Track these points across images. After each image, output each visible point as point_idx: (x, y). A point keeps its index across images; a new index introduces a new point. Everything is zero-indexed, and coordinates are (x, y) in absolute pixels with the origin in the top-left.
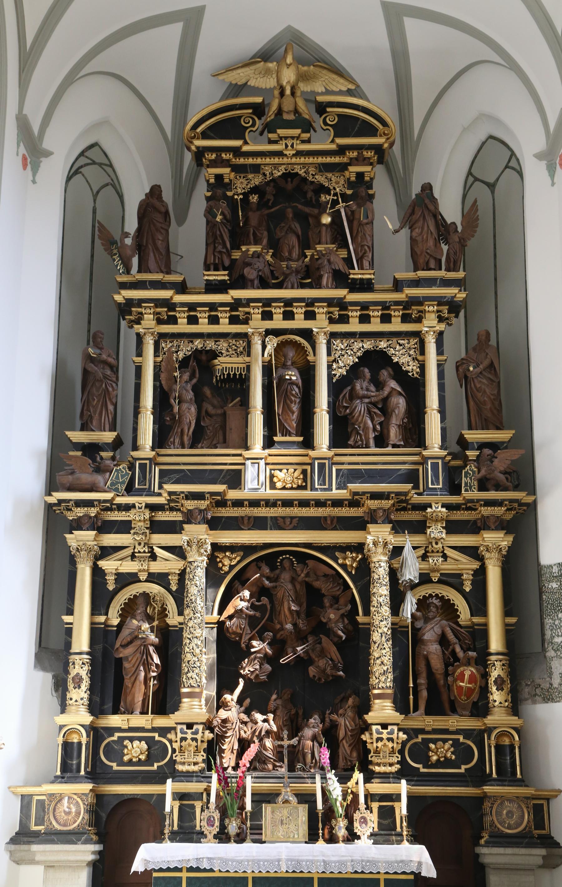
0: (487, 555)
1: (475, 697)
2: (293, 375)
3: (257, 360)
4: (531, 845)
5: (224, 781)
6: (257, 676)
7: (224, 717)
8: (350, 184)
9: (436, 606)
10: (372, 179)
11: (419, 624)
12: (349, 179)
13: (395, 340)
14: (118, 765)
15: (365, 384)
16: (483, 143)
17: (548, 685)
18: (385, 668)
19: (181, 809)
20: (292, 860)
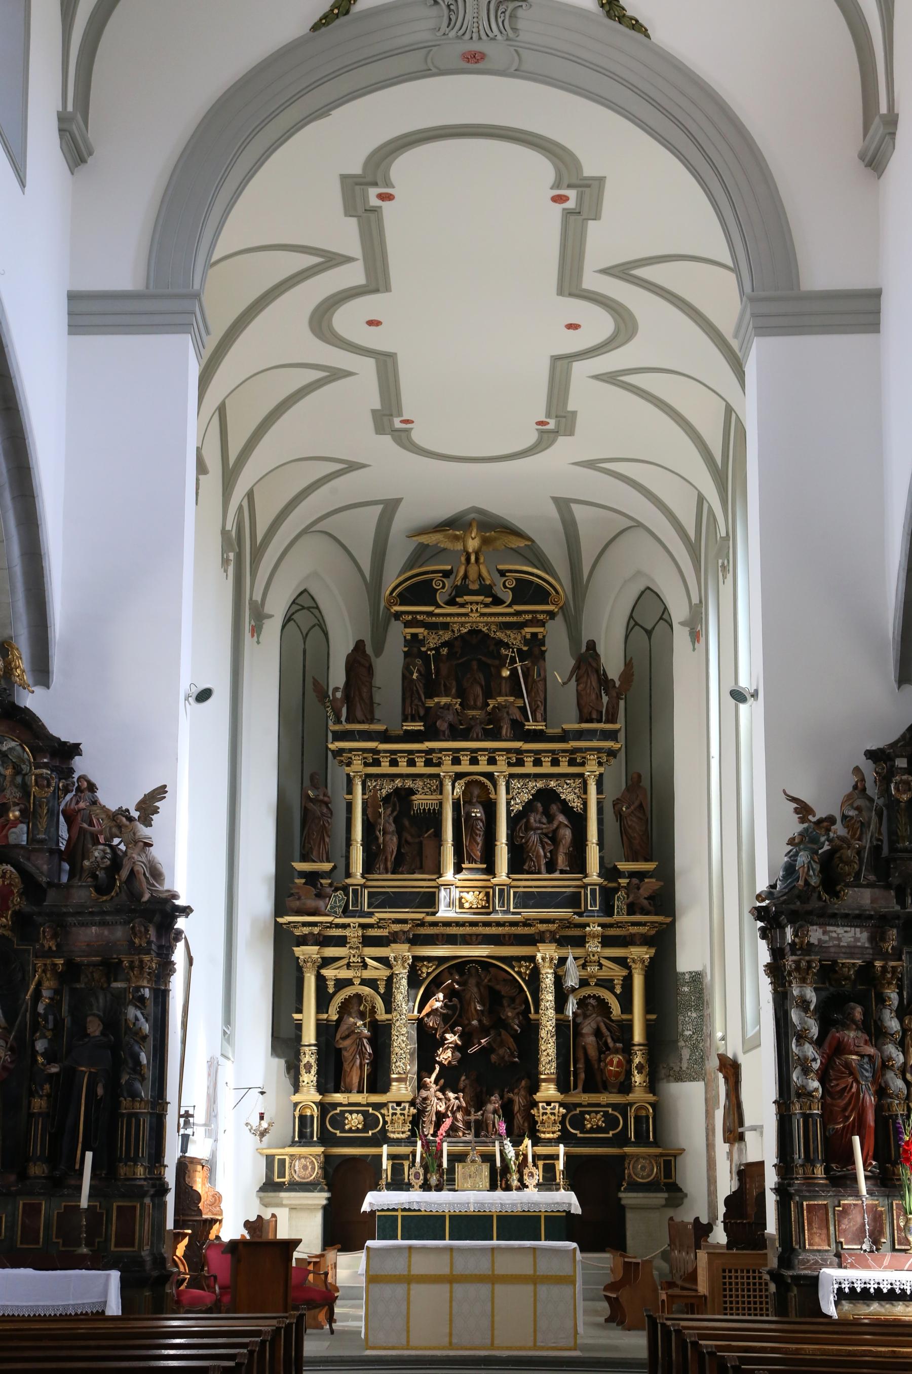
0: (633, 966)
1: (622, 1078)
2: (477, 812)
3: (448, 799)
4: (659, 1190)
5: (426, 1145)
6: (450, 1062)
7: (424, 1096)
8: (526, 642)
9: (593, 1006)
10: (544, 636)
11: (579, 1020)
12: (525, 636)
13: (563, 780)
14: (340, 1133)
15: (538, 817)
16: (643, 592)
17: (678, 1069)
18: (550, 1058)
19: (393, 1166)
20: (477, 1203)
